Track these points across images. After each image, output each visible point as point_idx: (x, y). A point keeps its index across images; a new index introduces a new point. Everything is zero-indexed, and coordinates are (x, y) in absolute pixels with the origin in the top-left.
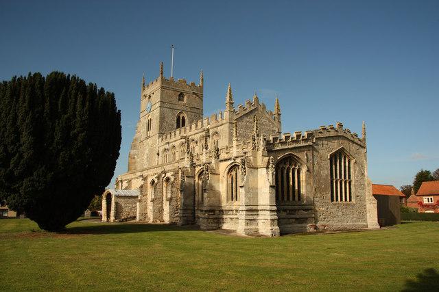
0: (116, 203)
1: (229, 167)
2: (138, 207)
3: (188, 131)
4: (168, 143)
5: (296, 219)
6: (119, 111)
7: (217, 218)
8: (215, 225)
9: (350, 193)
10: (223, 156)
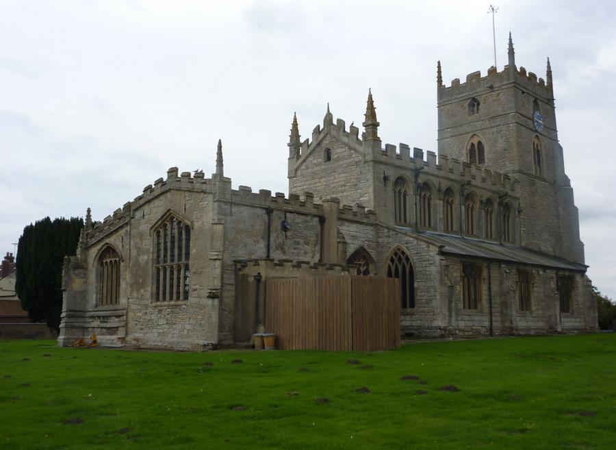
5: (110, 328)
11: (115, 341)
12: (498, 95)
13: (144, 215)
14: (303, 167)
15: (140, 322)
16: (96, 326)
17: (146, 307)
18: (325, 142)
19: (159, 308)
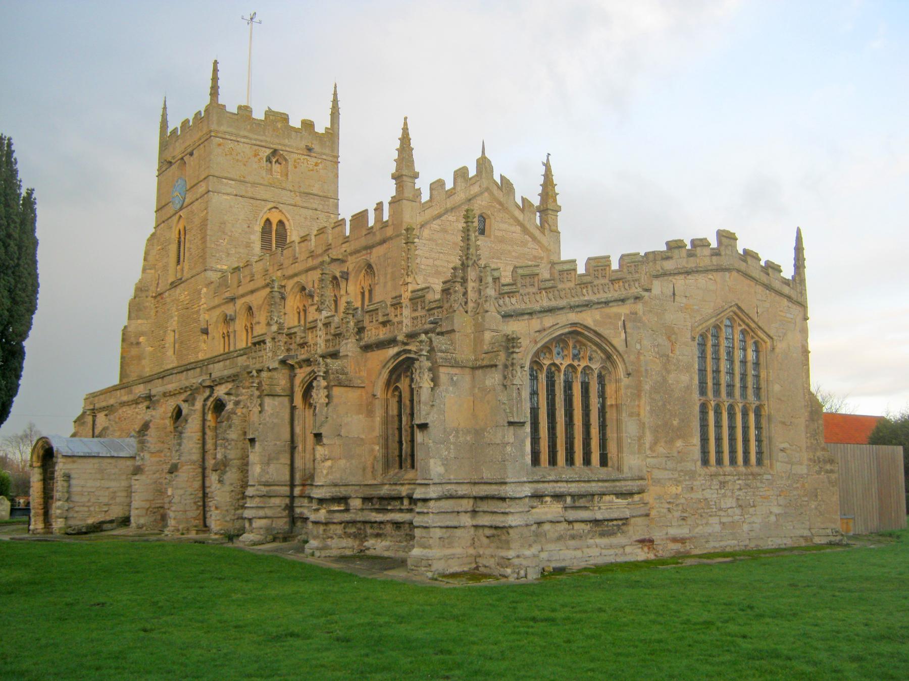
1: (391, 366)
4: (232, 300)
5: (596, 522)
6: (30, 193)
8: (349, 542)
9: (704, 440)
11: (628, 549)
13: (674, 294)
14: (435, 225)
17: (692, 475)
19: (721, 478)
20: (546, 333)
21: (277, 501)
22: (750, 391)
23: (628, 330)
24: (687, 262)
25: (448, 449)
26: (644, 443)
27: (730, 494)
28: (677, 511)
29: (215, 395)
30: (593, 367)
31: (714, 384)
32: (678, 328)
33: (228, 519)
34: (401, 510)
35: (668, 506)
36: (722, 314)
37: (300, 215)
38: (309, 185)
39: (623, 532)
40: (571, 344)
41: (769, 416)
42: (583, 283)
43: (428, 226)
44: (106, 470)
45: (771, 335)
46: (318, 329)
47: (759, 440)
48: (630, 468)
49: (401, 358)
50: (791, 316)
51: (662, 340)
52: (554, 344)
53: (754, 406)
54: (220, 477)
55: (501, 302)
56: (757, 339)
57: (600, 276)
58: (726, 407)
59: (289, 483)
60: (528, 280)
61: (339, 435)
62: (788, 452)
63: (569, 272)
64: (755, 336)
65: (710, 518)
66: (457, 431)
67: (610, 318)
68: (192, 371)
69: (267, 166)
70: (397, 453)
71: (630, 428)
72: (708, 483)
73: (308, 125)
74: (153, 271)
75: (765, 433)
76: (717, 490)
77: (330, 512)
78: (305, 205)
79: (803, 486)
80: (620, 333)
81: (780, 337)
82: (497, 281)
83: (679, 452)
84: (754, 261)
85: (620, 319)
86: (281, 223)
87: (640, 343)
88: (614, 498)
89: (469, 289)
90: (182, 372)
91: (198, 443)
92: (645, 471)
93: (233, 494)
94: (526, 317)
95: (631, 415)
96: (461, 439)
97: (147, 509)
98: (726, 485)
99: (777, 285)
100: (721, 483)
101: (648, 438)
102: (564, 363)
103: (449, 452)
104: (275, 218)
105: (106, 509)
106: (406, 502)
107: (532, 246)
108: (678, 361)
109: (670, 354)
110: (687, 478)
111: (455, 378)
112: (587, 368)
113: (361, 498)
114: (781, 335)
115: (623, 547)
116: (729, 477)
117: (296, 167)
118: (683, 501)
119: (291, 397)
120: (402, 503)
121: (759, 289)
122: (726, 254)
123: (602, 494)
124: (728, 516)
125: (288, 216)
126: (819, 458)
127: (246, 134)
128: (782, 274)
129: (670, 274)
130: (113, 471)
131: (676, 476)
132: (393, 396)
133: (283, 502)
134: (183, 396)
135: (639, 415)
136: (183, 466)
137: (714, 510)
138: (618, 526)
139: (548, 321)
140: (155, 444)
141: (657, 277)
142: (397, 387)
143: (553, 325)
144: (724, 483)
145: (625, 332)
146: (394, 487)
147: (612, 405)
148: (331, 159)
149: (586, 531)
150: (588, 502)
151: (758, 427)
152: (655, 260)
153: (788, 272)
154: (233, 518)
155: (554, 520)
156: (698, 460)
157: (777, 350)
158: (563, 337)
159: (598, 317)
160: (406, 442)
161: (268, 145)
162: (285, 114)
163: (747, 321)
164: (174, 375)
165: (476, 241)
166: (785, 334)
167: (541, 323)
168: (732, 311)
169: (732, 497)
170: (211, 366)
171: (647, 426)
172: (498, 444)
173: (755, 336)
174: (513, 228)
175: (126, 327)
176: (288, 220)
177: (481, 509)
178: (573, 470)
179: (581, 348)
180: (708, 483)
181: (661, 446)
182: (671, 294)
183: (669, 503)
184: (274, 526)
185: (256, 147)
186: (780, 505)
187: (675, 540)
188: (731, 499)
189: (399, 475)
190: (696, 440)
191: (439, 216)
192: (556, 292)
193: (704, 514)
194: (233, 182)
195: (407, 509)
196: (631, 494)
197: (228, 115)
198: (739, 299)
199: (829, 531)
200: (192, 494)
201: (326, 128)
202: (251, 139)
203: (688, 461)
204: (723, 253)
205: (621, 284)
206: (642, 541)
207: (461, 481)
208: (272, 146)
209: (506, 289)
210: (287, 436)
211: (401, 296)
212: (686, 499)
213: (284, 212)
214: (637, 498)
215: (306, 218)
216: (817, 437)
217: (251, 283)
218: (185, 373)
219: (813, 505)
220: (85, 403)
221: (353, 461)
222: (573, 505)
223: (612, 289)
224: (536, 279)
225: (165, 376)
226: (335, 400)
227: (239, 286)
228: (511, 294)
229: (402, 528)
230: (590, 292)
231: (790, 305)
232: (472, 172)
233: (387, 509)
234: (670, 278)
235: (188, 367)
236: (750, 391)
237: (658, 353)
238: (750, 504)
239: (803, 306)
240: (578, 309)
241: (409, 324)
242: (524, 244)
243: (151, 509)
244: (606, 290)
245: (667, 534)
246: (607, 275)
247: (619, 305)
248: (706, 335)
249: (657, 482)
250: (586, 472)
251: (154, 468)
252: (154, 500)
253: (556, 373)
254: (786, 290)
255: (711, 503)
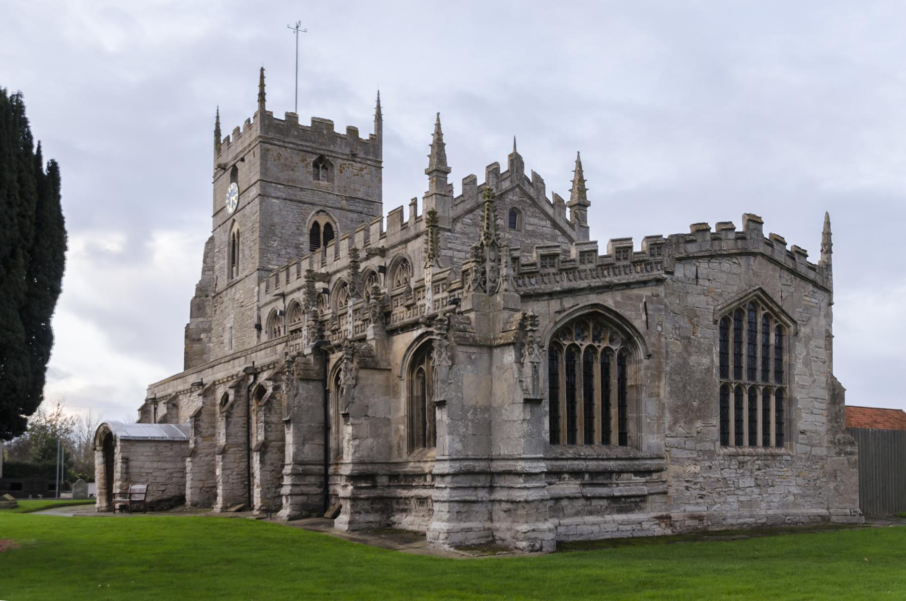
0: (126, 460)
2: (188, 469)
3: (329, 259)
5: (613, 499)
6: (54, 167)
7: (380, 499)
10: (400, 315)
12: (361, 169)
13: (697, 277)
14: (467, 220)
15: (695, 484)
16: (503, 499)
17: (711, 455)
18: (510, 197)
20: (566, 313)
21: (312, 479)
22: (772, 375)
23: (649, 312)
24: (712, 245)
25: (466, 426)
26: (664, 423)
27: (749, 474)
28: (695, 489)
29: (258, 382)
30: (614, 348)
31: (735, 367)
32: (700, 311)
33: (269, 496)
34: (424, 487)
35: (687, 484)
36: (746, 298)
37: (346, 218)
38: (355, 190)
39: (641, 509)
40: (591, 326)
41: (790, 398)
42: (606, 265)
43: (460, 220)
44: (162, 452)
45: (795, 319)
46: (348, 315)
47: (779, 423)
48: (649, 447)
49: (424, 340)
50: (816, 301)
51: (684, 322)
52: (574, 325)
53: (775, 389)
54: (261, 457)
55: (520, 282)
56: (780, 323)
57: (622, 257)
58: (747, 389)
59: (323, 462)
60: (548, 260)
61: (366, 415)
62: (808, 434)
63: (590, 253)
64: (778, 320)
65: (728, 497)
66: (475, 409)
67: (632, 300)
68: (238, 360)
69: (314, 171)
70: (421, 433)
71: (650, 407)
72: (727, 463)
73: (353, 131)
74: (211, 273)
75: (785, 415)
76: (736, 469)
77: (356, 488)
78: (351, 208)
79: (822, 467)
80: (641, 315)
81: (804, 321)
82: (517, 262)
83: (698, 433)
84: (781, 245)
85: (641, 301)
86: (328, 226)
87: (661, 325)
88: (633, 476)
89: (488, 269)
90: (229, 361)
91: (244, 427)
92: (664, 451)
93: (274, 473)
94: (546, 298)
95: (651, 396)
96: (479, 416)
97: (201, 488)
98: (745, 465)
99: (802, 270)
100: (740, 463)
101: (668, 418)
102: (584, 344)
103: (467, 429)
104: (322, 221)
105: (163, 489)
106: (429, 478)
107: (562, 240)
108: (699, 343)
109: (692, 337)
110: (706, 458)
111: (473, 357)
112: (607, 349)
113: (388, 475)
114: (805, 319)
115: (640, 523)
116: (748, 458)
117: (341, 172)
118: (701, 480)
119: (324, 382)
120: (425, 480)
121: (785, 274)
122: (751, 238)
123: (620, 472)
124: (746, 495)
125: (334, 218)
126: (839, 440)
127: (294, 141)
128: (808, 259)
129: (694, 258)
130: (169, 454)
131: (695, 455)
132: (418, 377)
133: (318, 480)
134: (231, 383)
135: (658, 395)
136: (229, 448)
137: (733, 489)
138: (636, 502)
139: (568, 302)
140: (208, 429)
141: (680, 260)
142: (421, 368)
143: (573, 306)
144: (743, 463)
145: (646, 314)
146: (418, 464)
147: (632, 386)
148: (375, 164)
149: (604, 507)
150: (607, 479)
151: (779, 410)
152: (678, 243)
153: (815, 257)
154: (274, 496)
155: (571, 495)
156: (717, 441)
157: (801, 334)
158: (584, 318)
159: (619, 299)
160: (430, 422)
161: (314, 151)
162: (329, 121)
163: (771, 305)
164: (222, 364)
165: (495, 221)
166: (809, 319)
167: (561, 304)
168: (756, 295)
169: (751, 476)
170: (253, 355)
171: (666, 405)
172: (515, 421)
173: (778, 320)
174: (543, 223)
175: (188, 325)
176: (335, 223)
177: (498, 485)
178: (593, 448)
179: (602, 330)
180: (727, 463)
181: (680, 426)
182: (694, 277)
183: (687, 481)
184: (309, 502)
185: (303, 153)
186: (799, 486)
187: (692, 517)
188: (749, 479)
189: (423, 453)
190: (716, 421)
191: (471, 211)
192: (577, 274)
193: (721, 493)
194: (282, 186)
195: (430, 485)
196: (649, 472)
197: (276, 122)
198: (763, 283)
199: (848, 511)
200: (238, 474)
201: (371, 134)
202: (297, 145)
203: (707, 441)
204: (748, 237)
205: (643, 266)
206: (660, 518)
207: (479, 457)
208: (318, 151)
209: (526, 269)
210: (321, 418)
211: (424, 279)
212: (704, 478)
213: (332, 215)
214: (655, 476)
215: (352, 221)
216: (838, 420)
217: (299, 280)
218: (232, 362)
219: (832, 485)
220: (148, 392)
221: (380, 440)
222: (591, 482)
223: (633, 271)
224: (556, 260)
225: (214, 366)
226: (361, 382)
227: (287, 284)
228: (531, 275)
229: (425, 505)
230: (611, 273)
231: (816, 290)
232: (504, 168)
233: (412, 486)
234: (694, 261)
235: (235, 356)
236: (772, 375)
237: (679, 335)
238: (768, 484)
239: (828, 291)
240: (599, 291)
241: (431, 306)
242: (554, 238)
243: (204, 489)
244: (628, 272)
245: (685, 511)
246: (629, 257)
247: (641, 287)
248: (729, 319)
249: (676, 461)
250: (604, 451)
251: (206, 450)
252: (207, 480)
253: (577, 353)
254: (812, 275)
255: (729, 482)
